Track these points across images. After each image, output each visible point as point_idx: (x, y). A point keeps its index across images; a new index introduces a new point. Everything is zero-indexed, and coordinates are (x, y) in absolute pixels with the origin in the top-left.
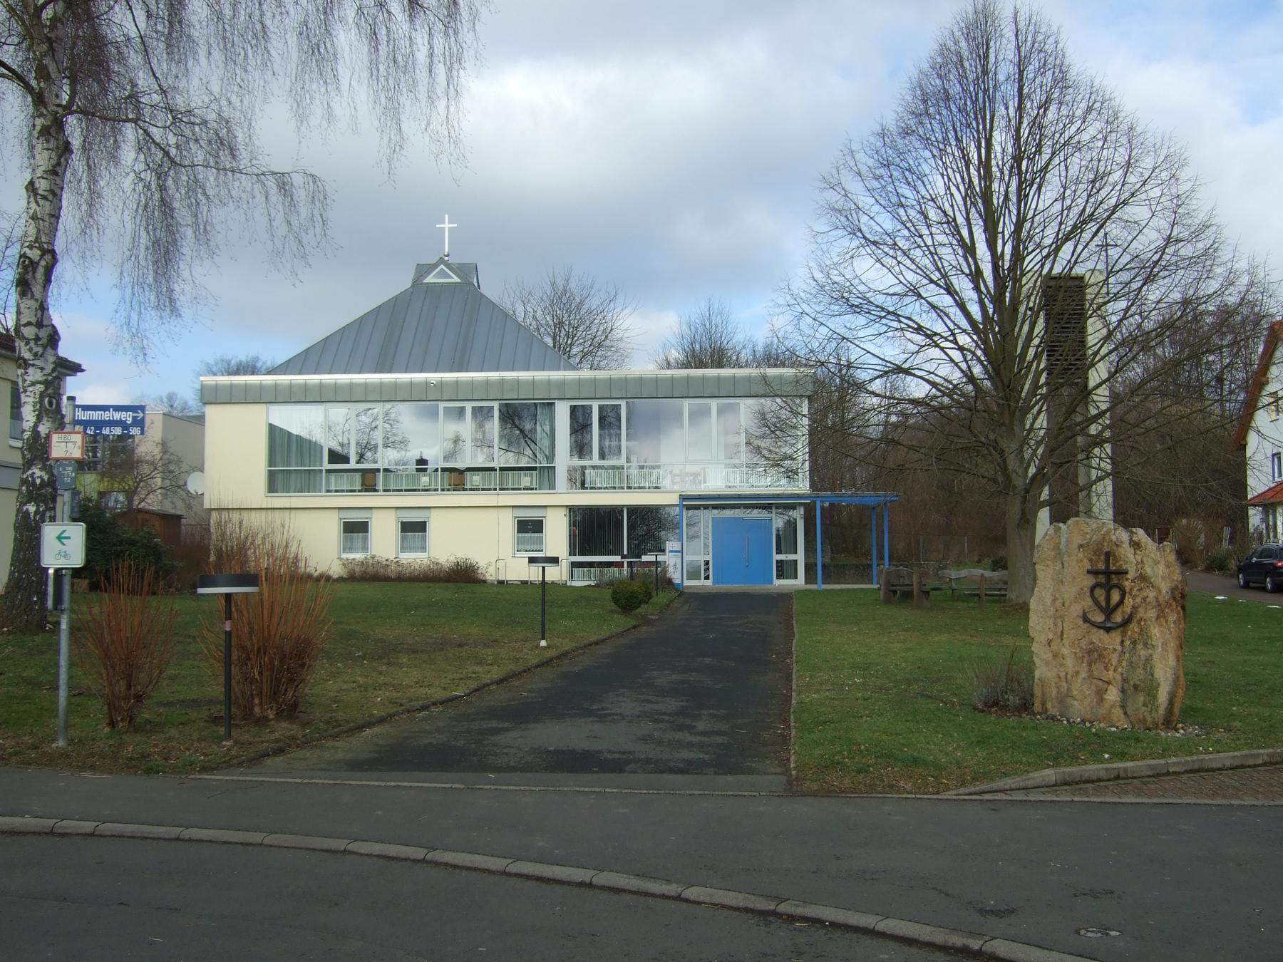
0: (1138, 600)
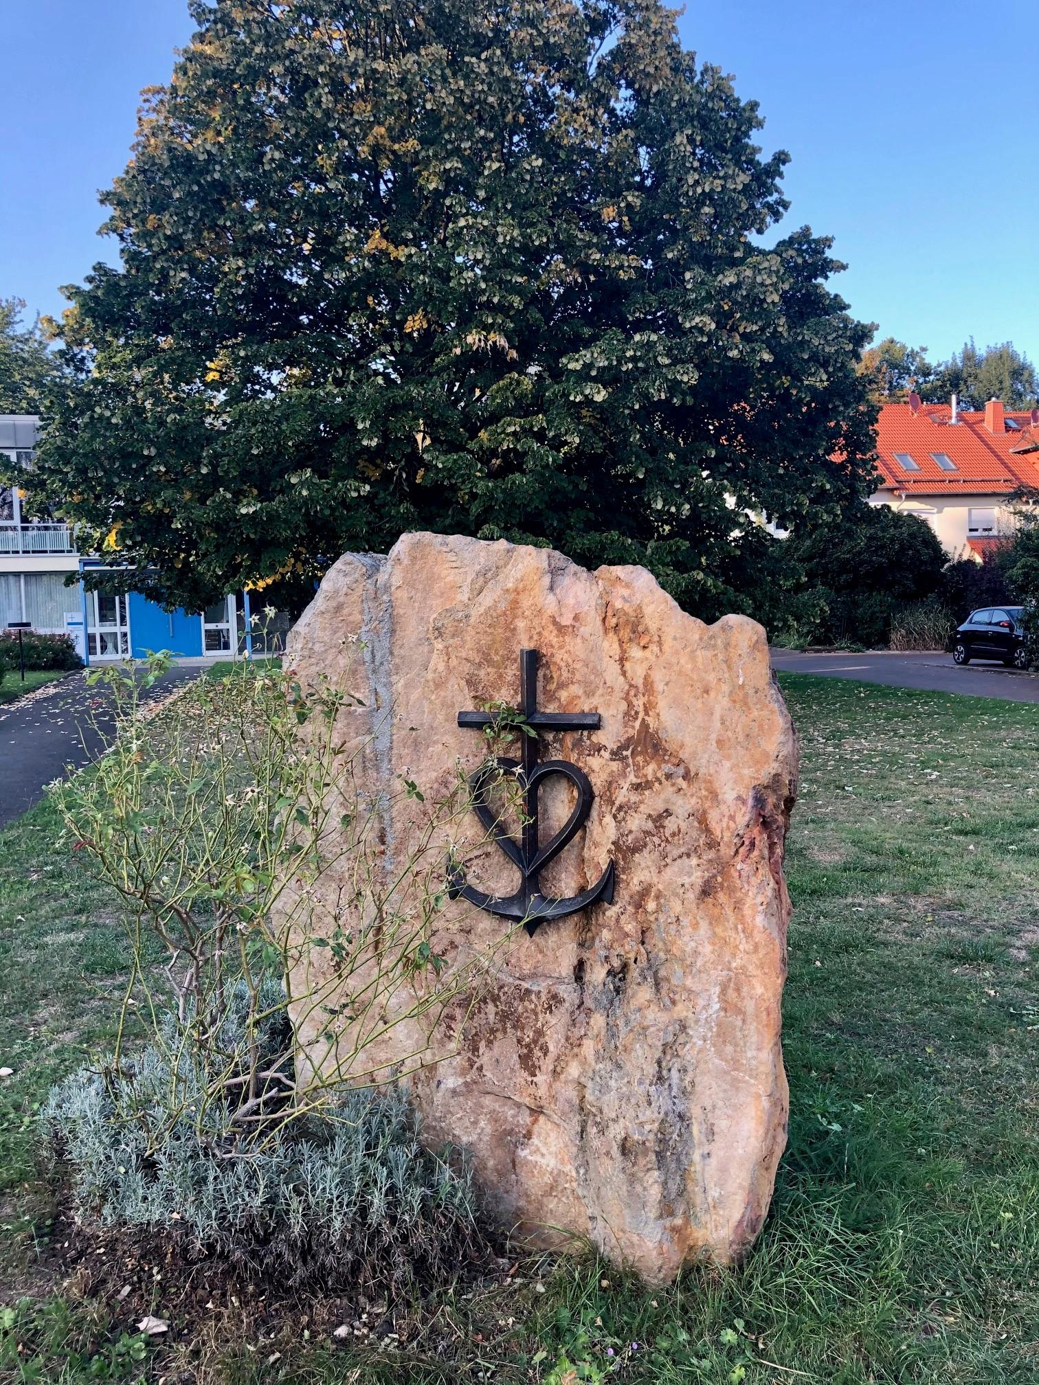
0: (636, 823)
